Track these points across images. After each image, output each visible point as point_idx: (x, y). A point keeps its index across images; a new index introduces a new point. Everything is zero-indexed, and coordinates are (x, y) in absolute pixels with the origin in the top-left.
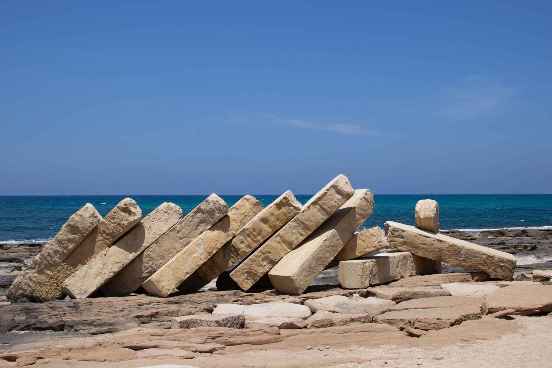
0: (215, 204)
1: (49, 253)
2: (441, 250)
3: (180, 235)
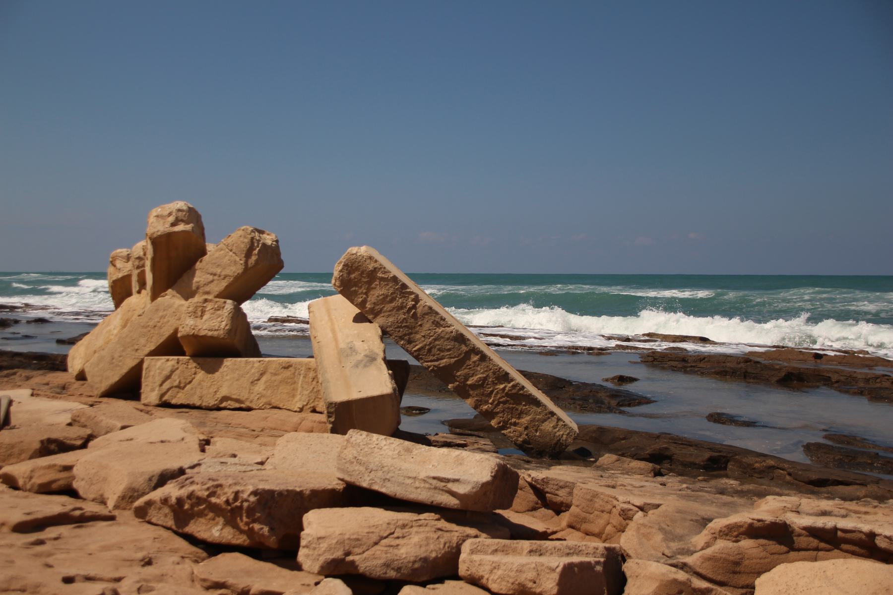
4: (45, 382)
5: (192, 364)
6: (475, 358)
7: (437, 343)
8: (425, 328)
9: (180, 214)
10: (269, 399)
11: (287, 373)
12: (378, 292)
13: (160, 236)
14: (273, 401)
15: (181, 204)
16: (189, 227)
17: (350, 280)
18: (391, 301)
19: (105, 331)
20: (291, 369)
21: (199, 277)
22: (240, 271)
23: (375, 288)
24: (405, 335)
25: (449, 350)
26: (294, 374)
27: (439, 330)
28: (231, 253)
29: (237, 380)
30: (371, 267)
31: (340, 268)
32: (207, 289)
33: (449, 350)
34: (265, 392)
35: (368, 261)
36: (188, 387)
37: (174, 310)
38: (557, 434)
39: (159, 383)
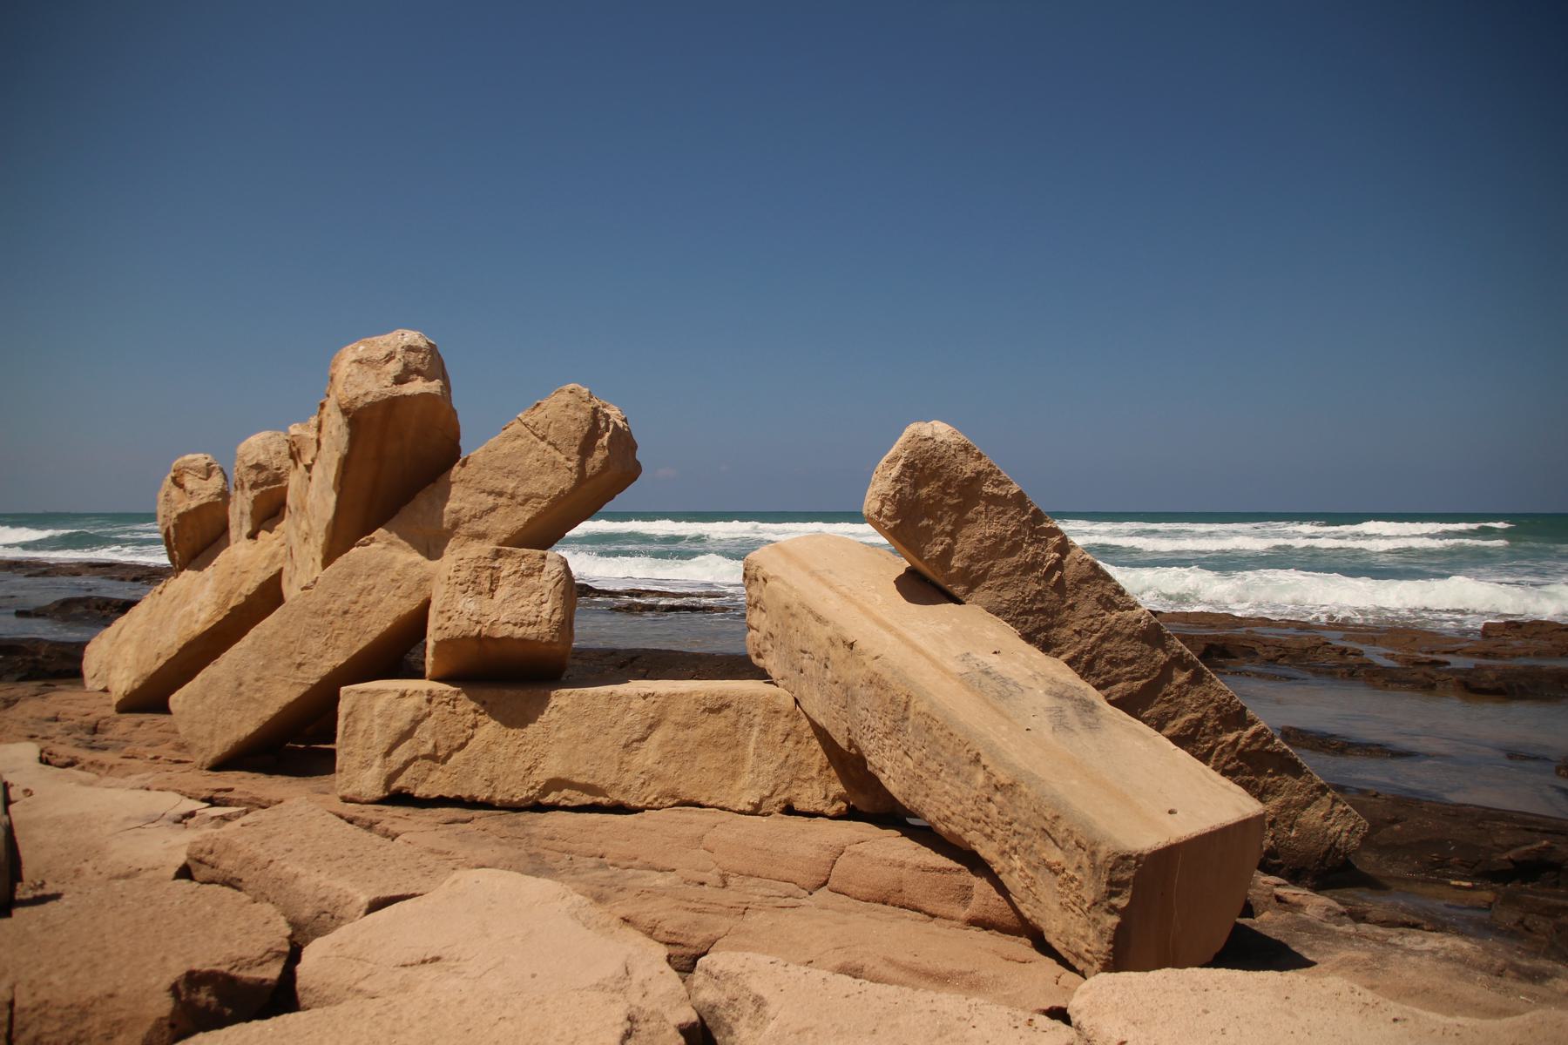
4: (49, 714)
5: (466, 705)
6: (1181, 677)
7: (1106, 645)
8: (1081, 614)
9: (412, 356)
10: (671, 785)
11: (718, 723)
12: (984, 528)
13: (372, 406)
14: (682, 788)
15: (411, 337)
16: (434, 386)
17: (917, 502)
18: (1011, 552)
19: (178, 614)
20: (726, 712)
21: (460, 499)
22: (567, 486)
23: (973, 521)
24: (1038, 630)
25: (1131, 662)
26: (735, 724)
27: (1112, 617)
28: (543, 445)
29: (587, 741)
30: (970, 467)
31: (895, 472)
32: (480, 526)
33: (1131, 662)
34: (661, 768)
35: (961, 456)
36: (456, 756)
37: (393, 575)
38: (1330, 832)
39: (384, 747)
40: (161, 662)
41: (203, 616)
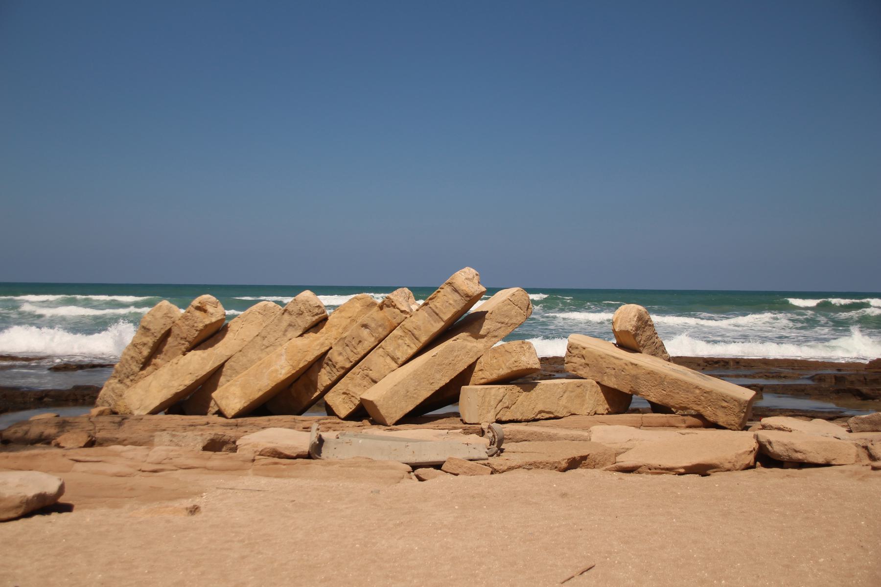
0: (304, 304)
1: (127, 360)
2: (635, 377)
3: (266, 342)
11: (579, 390)
40: (261, 393)
41: (284, 372)
